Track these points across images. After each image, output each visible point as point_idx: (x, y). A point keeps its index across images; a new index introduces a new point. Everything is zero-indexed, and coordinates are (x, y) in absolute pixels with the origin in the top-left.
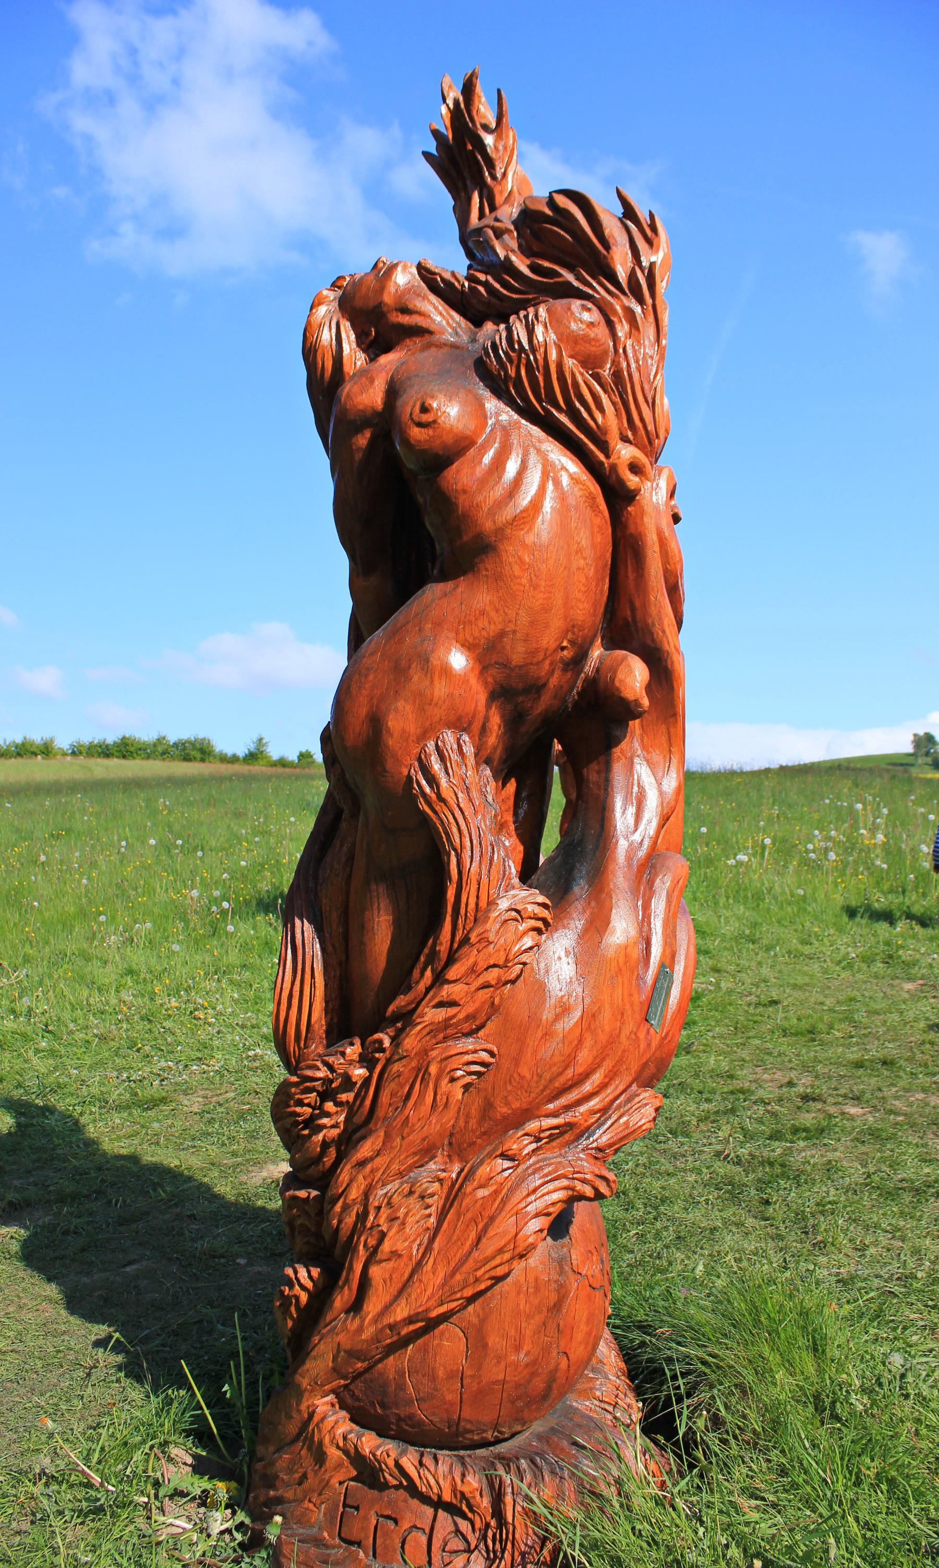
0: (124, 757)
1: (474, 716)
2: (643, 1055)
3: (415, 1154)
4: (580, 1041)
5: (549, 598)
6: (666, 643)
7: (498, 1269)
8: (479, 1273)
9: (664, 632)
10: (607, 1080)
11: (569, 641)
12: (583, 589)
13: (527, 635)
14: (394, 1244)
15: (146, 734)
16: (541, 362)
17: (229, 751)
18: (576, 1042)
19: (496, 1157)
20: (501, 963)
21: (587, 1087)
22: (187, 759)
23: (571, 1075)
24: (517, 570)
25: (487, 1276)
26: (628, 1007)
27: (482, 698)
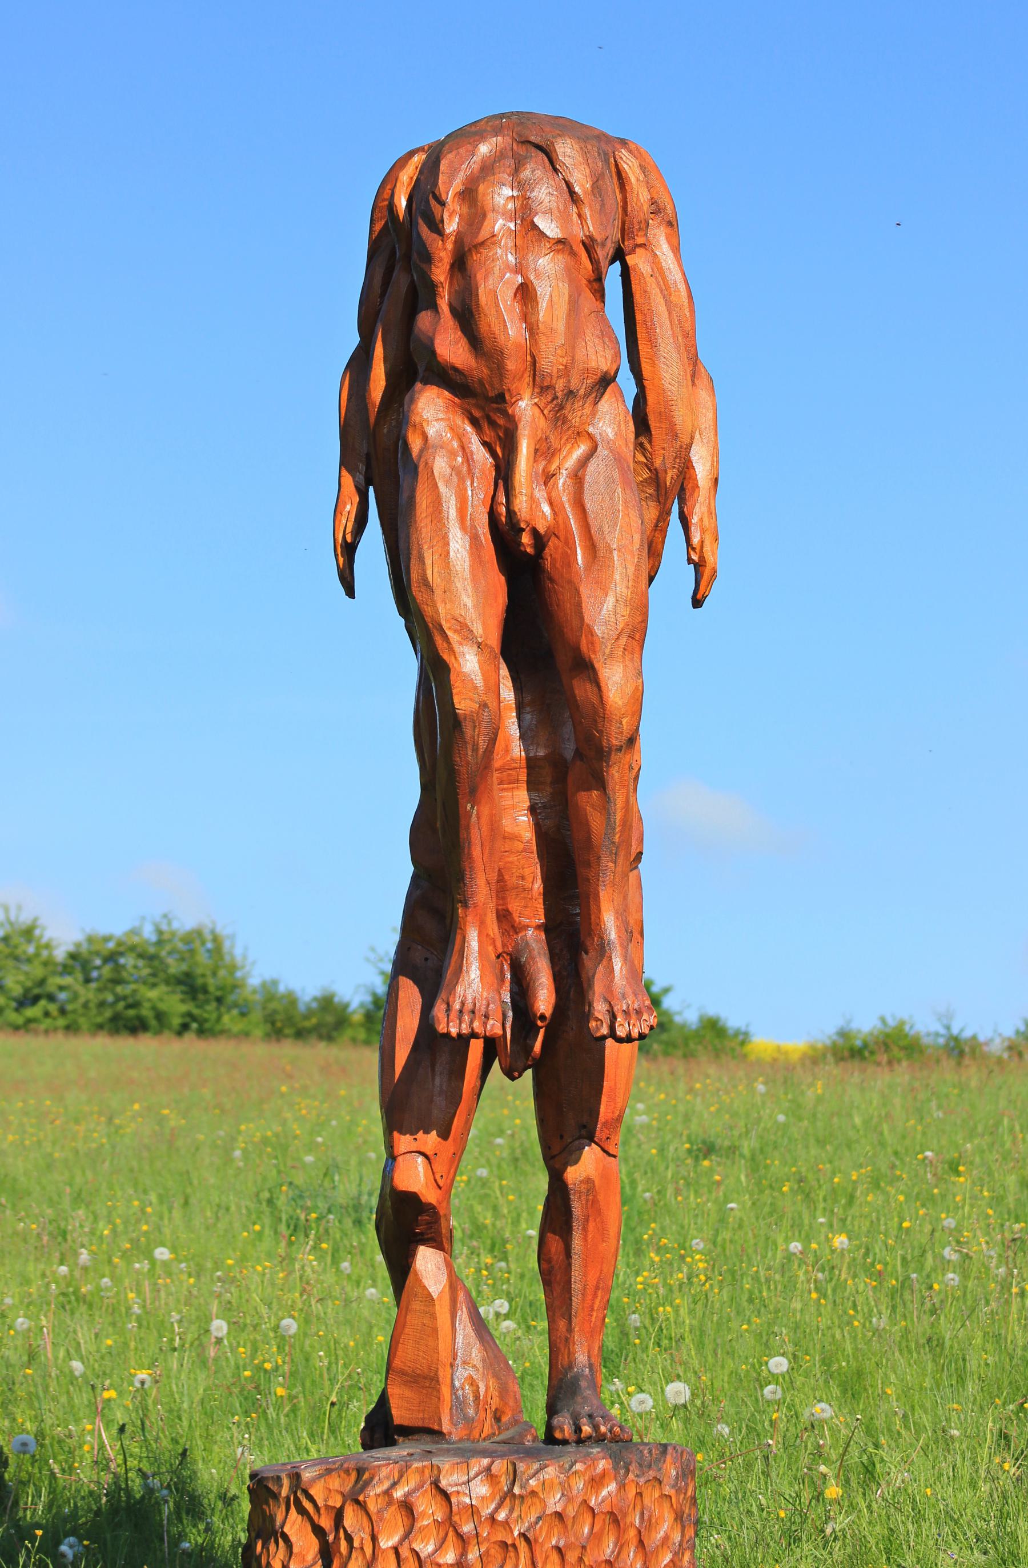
22: (129, 1023)
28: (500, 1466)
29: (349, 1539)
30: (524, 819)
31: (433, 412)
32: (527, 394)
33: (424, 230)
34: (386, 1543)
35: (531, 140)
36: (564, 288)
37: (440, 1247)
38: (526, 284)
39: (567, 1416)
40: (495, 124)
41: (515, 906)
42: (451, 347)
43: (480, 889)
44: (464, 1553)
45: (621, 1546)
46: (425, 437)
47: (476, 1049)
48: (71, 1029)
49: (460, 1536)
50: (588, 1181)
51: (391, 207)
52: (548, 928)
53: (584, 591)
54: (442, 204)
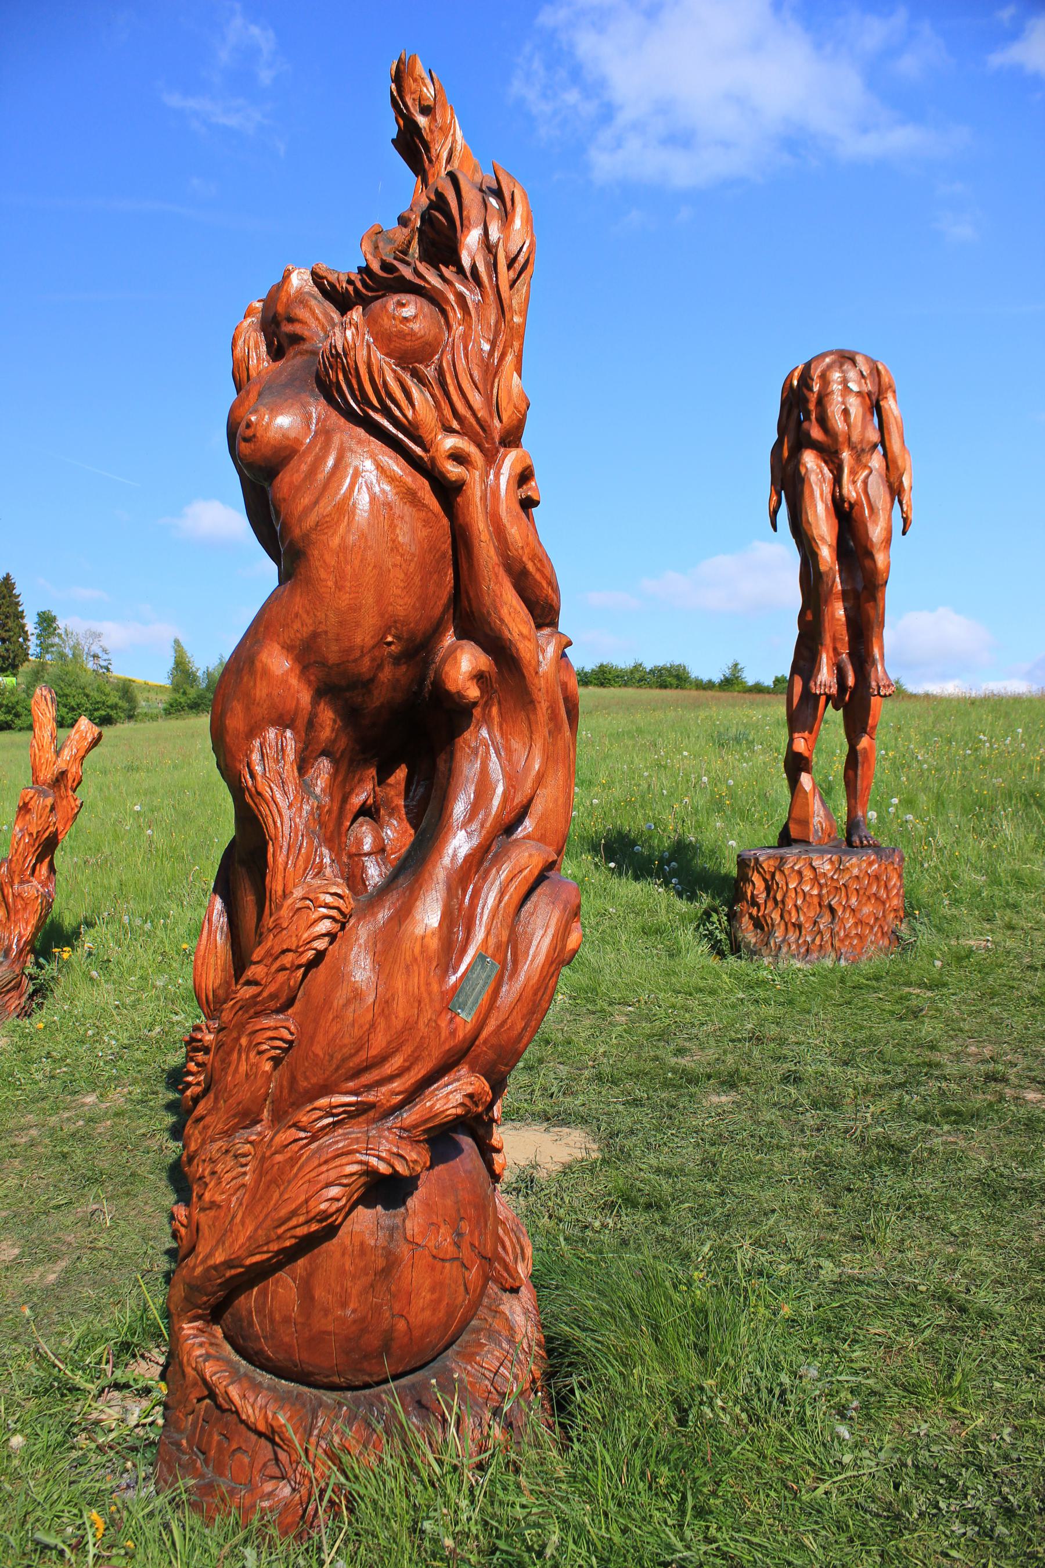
0: (602, 685)
1: (296, 713)
2: (444, 1042)
3: (234, 1116)
4: (373, 1025)
5: (356, 598)
6: (507, 632)
7: (298, 1229)
8: (280, 1231)
9: (501, 620)
10: (407, 1064)
11: (394, 636)
12: (402, 585)
13: (338, 635)
14: (212, 1196)
15: (623, 662)
16: (352, 364)
17: (705, 677)
18: (367, 1026)
19: (290, 1127)
20: (294, 948)
21: (388, 1069)
22: (663, 686)
23: (364, 1057)
24: (323, 574)
25: (289, 1234)
26: (425, 995)
27: (305, 697)
28: (834, 858)
29: (777, 884)
30: (842, 612)
31: (810, 460)
32: (846, 450)
33: (805, 391)
34: (792, 886)
35: (846, 358)
36: (861, 410)
37: (809, 773)
38: (845, 408)
39: (853, 837)
40: (831, 353)
41: (839, 646)
42: (816, 433)
43: (828, 640)
44: (821, 890)
45: (878, 887)
46: (807, 468)
47: (823, 699)
48: (651, 687)
49: (819, 884)
50: (864, 749)
51: (791, 384)
52: (850, 655)
53: (868, 524)
54: (812, 380)
